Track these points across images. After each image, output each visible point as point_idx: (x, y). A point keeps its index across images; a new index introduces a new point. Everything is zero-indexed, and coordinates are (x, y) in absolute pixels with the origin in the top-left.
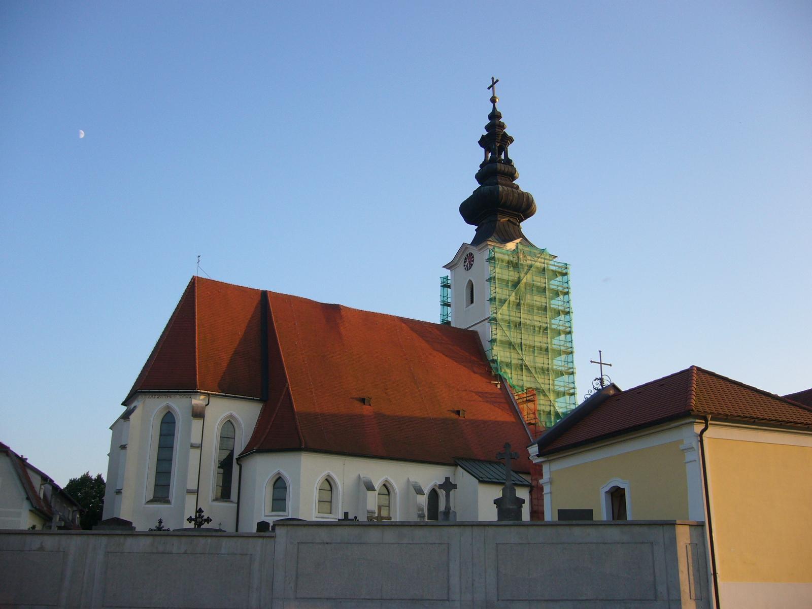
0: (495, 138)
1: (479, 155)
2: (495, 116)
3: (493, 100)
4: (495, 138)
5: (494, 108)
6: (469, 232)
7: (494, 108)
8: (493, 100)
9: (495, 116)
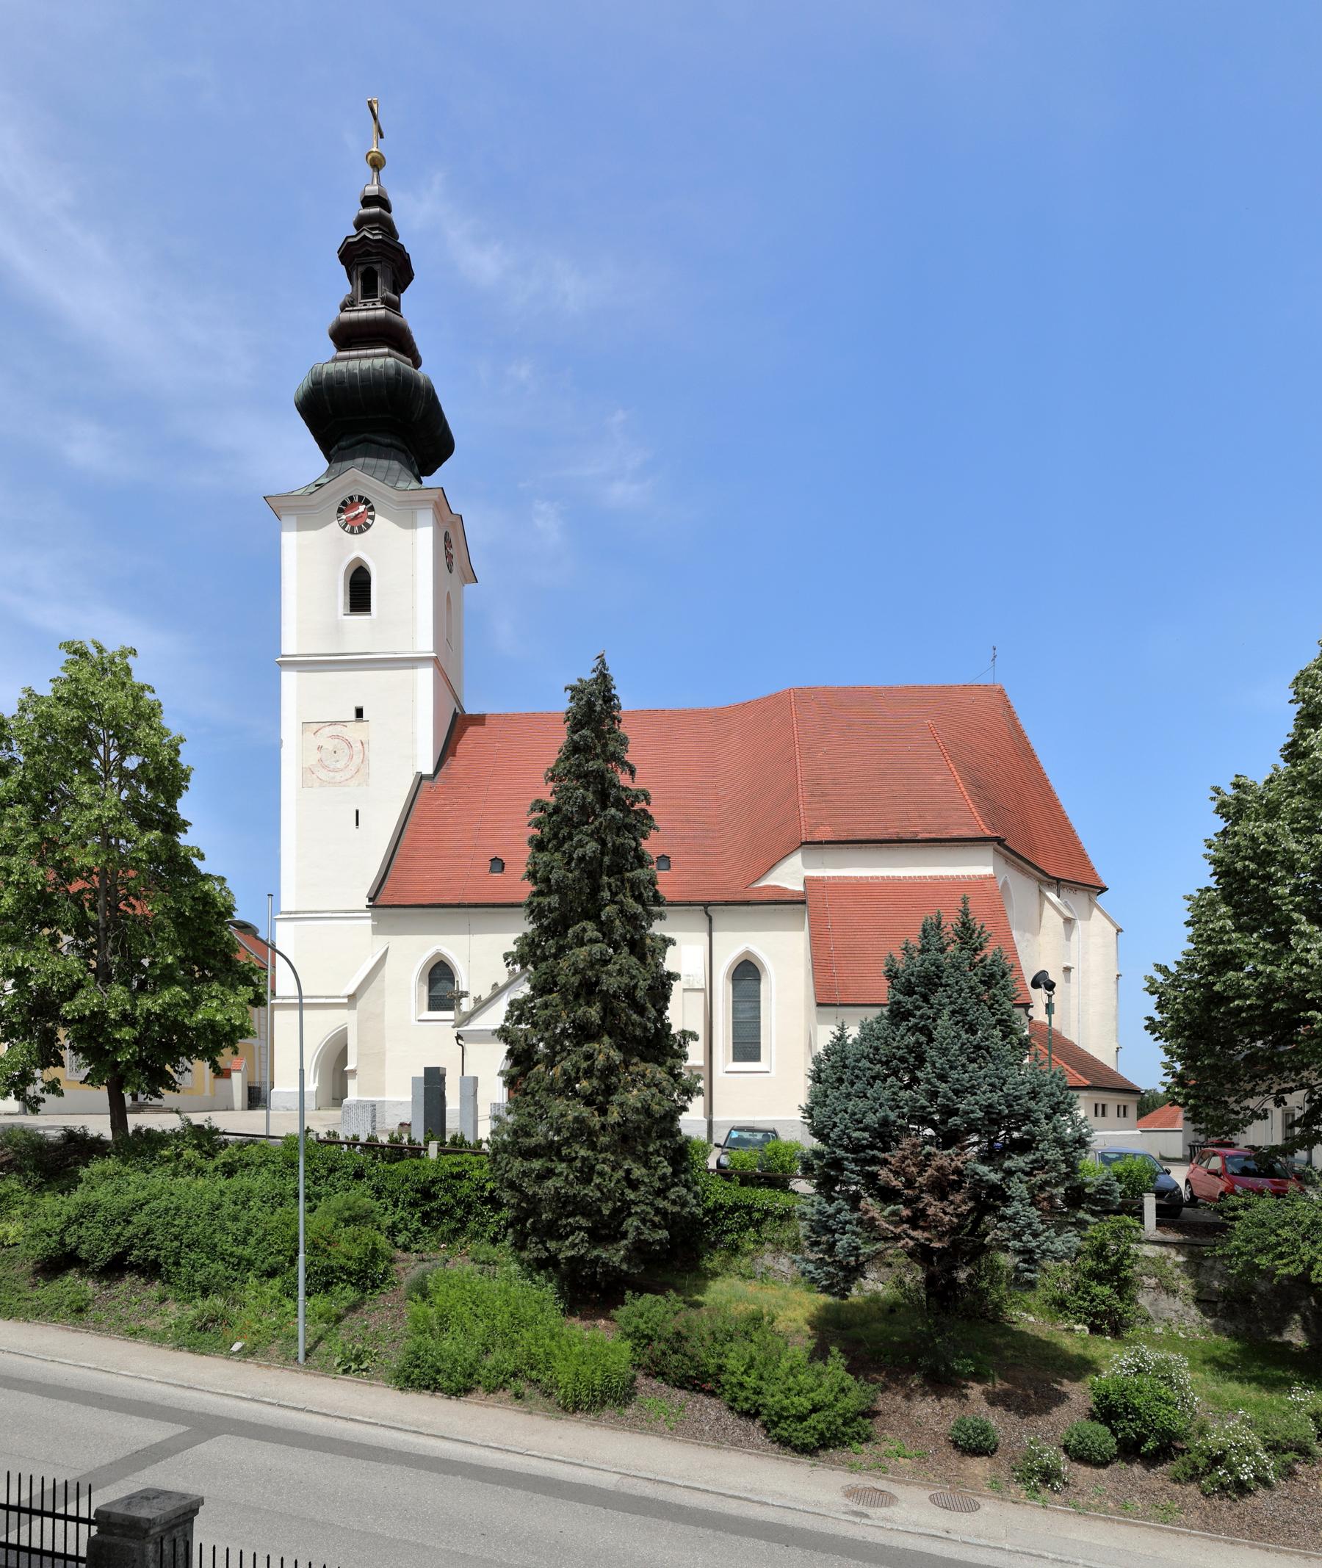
5: (1050, 996)
7: (1050, 996)
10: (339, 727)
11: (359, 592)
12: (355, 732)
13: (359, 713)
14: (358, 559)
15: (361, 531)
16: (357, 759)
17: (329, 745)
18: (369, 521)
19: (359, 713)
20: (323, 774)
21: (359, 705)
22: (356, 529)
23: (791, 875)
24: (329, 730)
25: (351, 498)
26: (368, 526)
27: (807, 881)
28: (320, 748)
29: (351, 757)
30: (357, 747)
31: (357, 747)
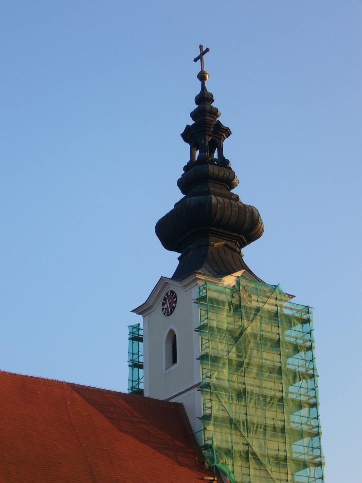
0: (205, 130)
1: (183, 154)
2: (204, 99)
3: (202, 77)
4: (205, 130)
5: (203, 88)
6: (169, 261)
7: (203, 88)
8: (202, 77)
9: (204, 99)
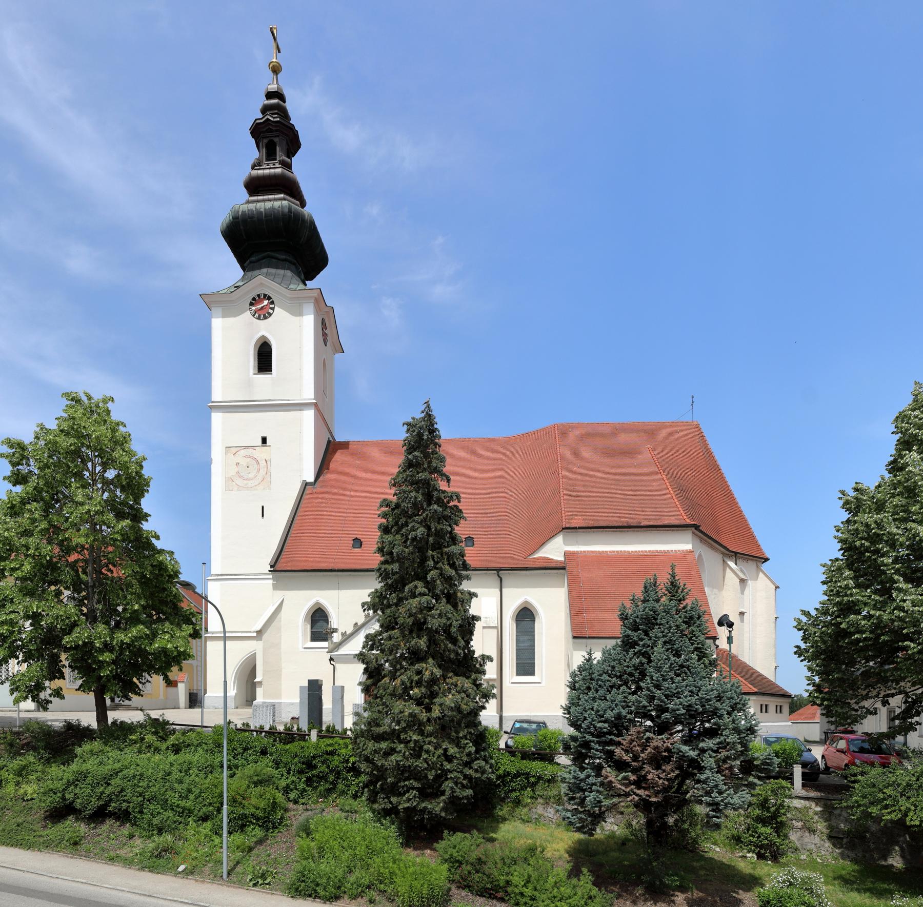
0: (276, 133)
10: (250, 450)
11: (264, 358)
12: (261, 453)
13: (264, 440)
14: (263, 337)
15: (265, 318)
16: (263, 472)
17: (244, 462)
18: (271, 311)
19: (264, 440)
20: (240, 482)
21: (264, 435)
22: (262, 317)
23: (555, 549)
24: (243, 452)
25: (259, 296)
26: (270, 315)
27: (567, 554)
28: (238, 464)
29: (259, 470)
30: (263, 463)
31: (263, 463)
